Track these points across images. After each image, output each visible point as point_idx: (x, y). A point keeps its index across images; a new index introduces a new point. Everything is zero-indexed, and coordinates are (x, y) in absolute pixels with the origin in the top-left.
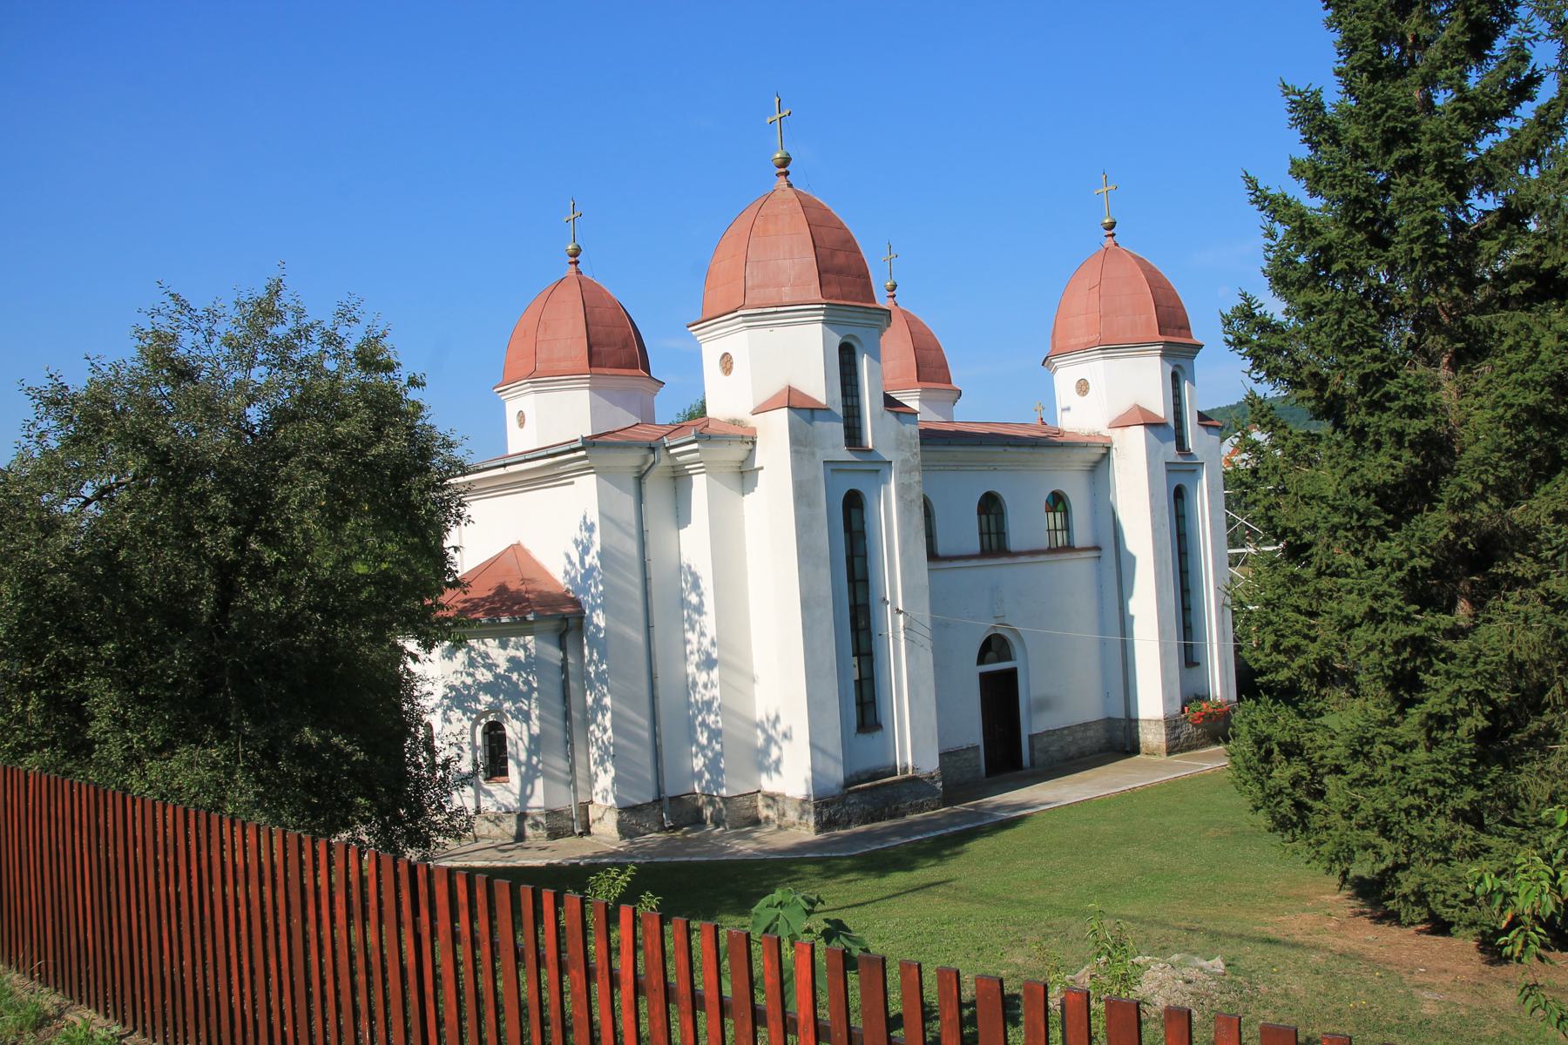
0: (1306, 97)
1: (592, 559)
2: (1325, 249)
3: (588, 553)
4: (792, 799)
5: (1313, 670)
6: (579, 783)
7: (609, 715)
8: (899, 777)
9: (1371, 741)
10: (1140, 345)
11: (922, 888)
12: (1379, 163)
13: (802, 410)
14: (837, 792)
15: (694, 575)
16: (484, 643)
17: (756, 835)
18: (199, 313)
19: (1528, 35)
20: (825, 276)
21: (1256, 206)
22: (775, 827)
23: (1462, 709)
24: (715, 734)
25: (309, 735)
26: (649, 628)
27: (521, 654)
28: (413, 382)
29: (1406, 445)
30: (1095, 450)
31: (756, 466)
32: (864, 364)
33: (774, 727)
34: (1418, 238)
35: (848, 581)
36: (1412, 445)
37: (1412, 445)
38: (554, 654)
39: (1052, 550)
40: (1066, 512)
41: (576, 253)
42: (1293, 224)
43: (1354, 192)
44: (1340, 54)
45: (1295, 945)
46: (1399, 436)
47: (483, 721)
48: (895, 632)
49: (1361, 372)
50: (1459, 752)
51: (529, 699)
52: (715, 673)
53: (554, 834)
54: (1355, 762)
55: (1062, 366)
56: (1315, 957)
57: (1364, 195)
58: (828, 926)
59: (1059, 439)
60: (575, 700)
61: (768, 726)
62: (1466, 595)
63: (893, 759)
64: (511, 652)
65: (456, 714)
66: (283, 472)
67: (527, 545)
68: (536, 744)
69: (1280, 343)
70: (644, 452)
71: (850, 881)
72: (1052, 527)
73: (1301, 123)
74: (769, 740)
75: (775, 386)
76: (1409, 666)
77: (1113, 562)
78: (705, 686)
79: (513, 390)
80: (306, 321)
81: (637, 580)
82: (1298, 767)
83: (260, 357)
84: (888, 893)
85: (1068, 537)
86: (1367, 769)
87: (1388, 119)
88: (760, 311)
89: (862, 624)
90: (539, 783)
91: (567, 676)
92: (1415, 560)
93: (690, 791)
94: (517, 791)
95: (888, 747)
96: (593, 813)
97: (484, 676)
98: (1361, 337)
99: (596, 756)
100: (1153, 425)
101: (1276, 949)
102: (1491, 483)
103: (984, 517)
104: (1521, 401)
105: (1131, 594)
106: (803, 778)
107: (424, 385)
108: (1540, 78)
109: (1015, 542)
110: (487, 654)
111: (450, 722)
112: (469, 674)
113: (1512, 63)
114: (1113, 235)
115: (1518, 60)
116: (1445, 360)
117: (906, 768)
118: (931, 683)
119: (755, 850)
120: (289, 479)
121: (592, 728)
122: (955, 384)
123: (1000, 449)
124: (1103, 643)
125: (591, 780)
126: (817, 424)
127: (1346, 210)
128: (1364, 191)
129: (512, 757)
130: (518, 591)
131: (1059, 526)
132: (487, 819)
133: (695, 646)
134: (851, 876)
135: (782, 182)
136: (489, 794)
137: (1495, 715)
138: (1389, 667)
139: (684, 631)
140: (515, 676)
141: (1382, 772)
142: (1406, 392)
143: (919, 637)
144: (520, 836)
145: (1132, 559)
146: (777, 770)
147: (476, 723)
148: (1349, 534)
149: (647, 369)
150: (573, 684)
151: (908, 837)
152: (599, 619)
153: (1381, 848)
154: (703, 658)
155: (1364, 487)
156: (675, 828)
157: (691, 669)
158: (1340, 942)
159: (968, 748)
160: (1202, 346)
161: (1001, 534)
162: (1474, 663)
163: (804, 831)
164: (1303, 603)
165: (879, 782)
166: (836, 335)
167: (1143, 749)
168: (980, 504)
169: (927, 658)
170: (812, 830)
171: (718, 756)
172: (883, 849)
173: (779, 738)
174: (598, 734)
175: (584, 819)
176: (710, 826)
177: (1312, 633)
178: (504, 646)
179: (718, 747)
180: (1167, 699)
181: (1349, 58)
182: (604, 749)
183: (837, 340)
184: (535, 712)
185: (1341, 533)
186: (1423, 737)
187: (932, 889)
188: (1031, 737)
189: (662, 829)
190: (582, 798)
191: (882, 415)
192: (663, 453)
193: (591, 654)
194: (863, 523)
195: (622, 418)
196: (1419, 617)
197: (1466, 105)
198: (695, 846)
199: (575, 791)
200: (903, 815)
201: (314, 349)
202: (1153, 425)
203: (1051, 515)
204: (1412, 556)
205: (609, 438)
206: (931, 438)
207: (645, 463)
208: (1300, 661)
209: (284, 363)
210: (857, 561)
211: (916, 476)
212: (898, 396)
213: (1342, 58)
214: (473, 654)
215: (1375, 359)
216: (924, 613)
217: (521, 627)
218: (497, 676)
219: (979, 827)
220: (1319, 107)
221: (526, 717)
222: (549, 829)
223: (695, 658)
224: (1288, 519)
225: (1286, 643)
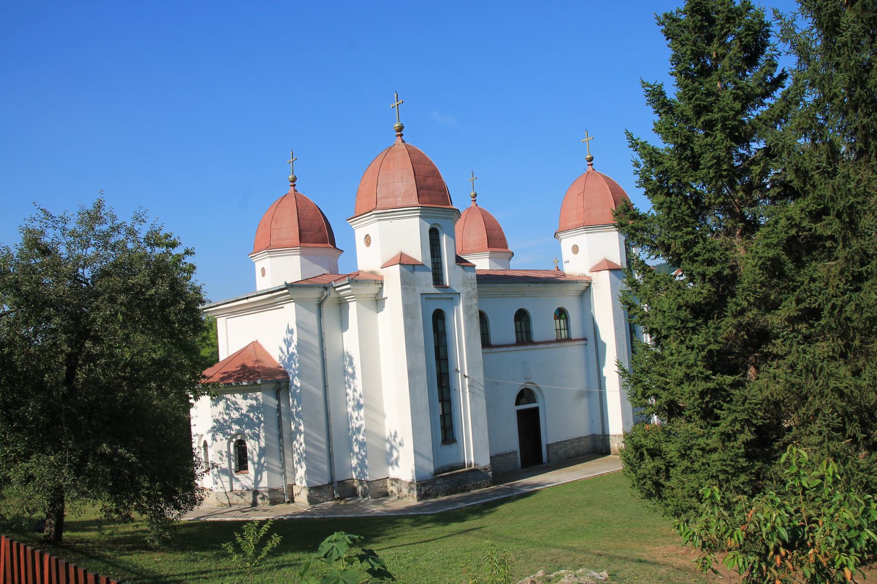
1: (292, 349)
3: (290, 346)
4: (405, 482)
5: (664, 408)
6: (287, 474)
7: (303, 436)
8: (466, 469)
9: (690, 448)
11: (466, 531)
13: (407, 265)
14: (430, 478)
15: (350, 357)
16: (234, 396)
17: (385, 502)
19: (775, 53)
20: (421, 191)
21: (632, 149)
23: (737, 430)
24: (362, 445)
25: (105, 448)
26: (325, 387)
27: (254, 402)
28: (187, 252)
30: (581, 285)
31: (384, 297)
32: (444, 239)
34: (712, 166)
35: (436, 360)
36: (711, 280)
38: (273, 402)
39: (558, 341)
40: (567, 319)
41: (294, 180)
43: (679, 141)
44: (672, 65)
46: (703, 276)
47: (234, 440)
49: (682, 240)
50: (735, 455)
51: (259, 427)
52: (362, 412)
53: (273, 502)
55: (565, 238)
56: (663, 570)
59: (563, 279)
61: (391, 439)
62: (753, 364)
65: (220, 436)
67: (261, 342)
68: (262, 452)
70: (321, 290)
72: (558, 327)
74: (392, 447)
75: (394, 253)
76: (710, 405)
77: (594, 348)
78: (357, 419)
80: (118, 222)
81: (318, 360)
82: (659, 463)
83: (93, 242)
84: (446, 534)
85: (568, 333)
86: (689, 464)
87: (696, 100)
88: (384, 211)
89: (444, 384)
90: (265, 474)
91: (280, 415)
94: (253, 478)
95: (460, 452)
96: (296, 490)
97: (235, 415)
98: (682, 222)
100: (614, 270)
101: (643, 566)
103: (518, 323)
104: (766, 255)
105: (604, 365)
107: (194, 253)
108: (787, 76)
109: (536, 336)
111: (216, 441)
112: (227, 414)
113: (767, 68)
114: (592, 165)
115: (770, 66)
116: (738, 233)
117: (471, 464)
119: (382, 511)
120: (98, 308)
121: (295, 442)
122: (510, 248)
123: (526, 285)
125: (294, 471)
126: (417, 273)
127: (677, 149)
129: (250, 460)
130: (254, 367)
131: (562, 327)
132: (236, 494)
133: (352, 397)
134: (428, 525)
135: (399, 140)
136: (237, 480)
137: (759, 430)
138: (698, 406)
139: (346, 389)
140: (251, 415)
141: (696, 466)
143: (477, 391)
144: (254, 504)
145: (604, 345)
146: (397, 464)
147: (230, 441)
148: (678, 332)
149: (333, 243)
150: (284, 418)
151: (469, 503)
152: (297, 382)
154: (356, 403)
155: (685, 305)
156: (341, 499)
157: (350, 410)
158: (680, 561)
161: (528, 332)
162: (743, 403)
165: (454, 472)
167: (612, 452)
169: (482, 402)
170: (416, 499)
174: (297, 446)
175: (291, 493)
177: (667, 387)
178: (245, 398)
180: (625, 423)
182: (300, 455)
183: (428, 226)
184: (262, 434)
186: (721, 445)
187: (471, 532)
188: (548, 446)
189: (334, 499)
190: (289, 482)
191: (455, 267)
192: (332, 290)
193: (293, 402)
194: (445, 327)
195: (318, 270)
196: (714, 377)
197: (738, 91)
198: (350, 509)
199: (285, 478)
200: (469, 490)
201: (122, 237)
203: (558, 321)
204: (709, 343)
206: (484, 279)
207: (322, 296)
209: (105, 245)
210: (441, 349)
211: (475, 301)
215: (688, 233)
216: (480, 377)
217: (254, 387)
218: (242, 414)
219: (510, 497)
220: (662, 93)
221: (257, 437)
222: (270, 499)
223: (351, 403)
224: (653, 323)
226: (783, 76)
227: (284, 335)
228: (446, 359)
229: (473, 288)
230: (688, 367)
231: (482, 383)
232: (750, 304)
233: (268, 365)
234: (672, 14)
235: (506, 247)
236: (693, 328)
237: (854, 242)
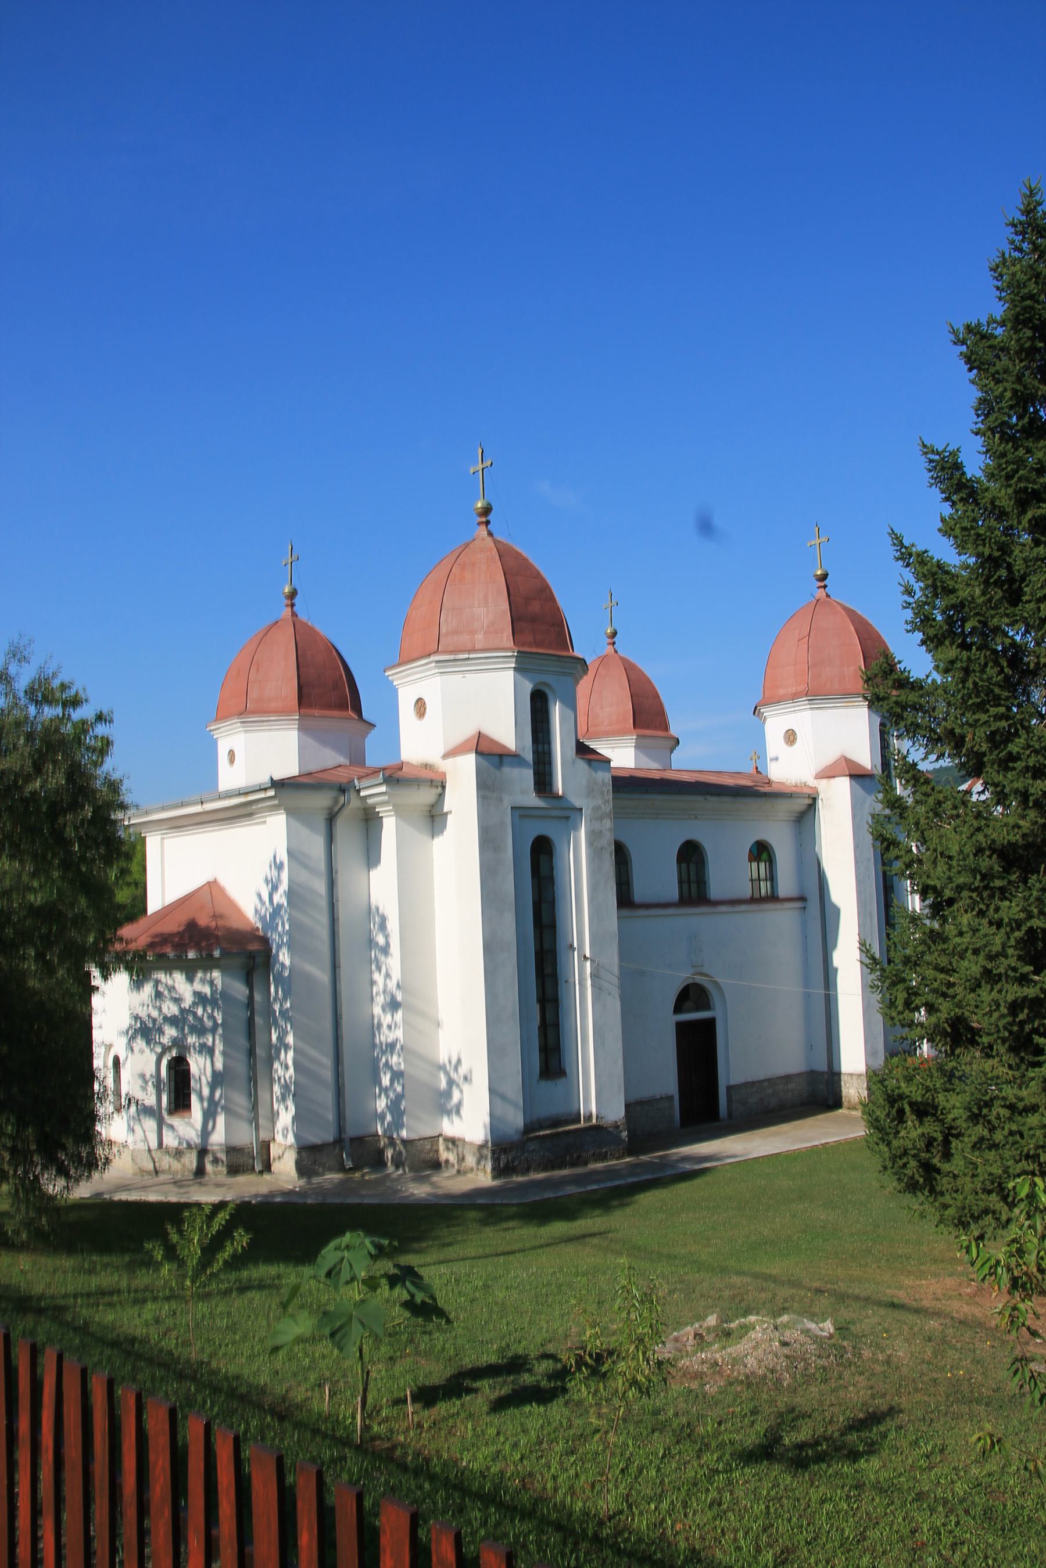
0: (944, 457)
1: (280, 898)
2: (959, 607)
4: (471, 1144)
6: (261, 1121)
7: (291, 1054)
9: (989, 1104)
10: (845, 695)
12: (1015, 523)
14: (516, 1138)
21: (901, 563)
22: (454, 1171)
26: (335, 967)
27: (207, 990)
29: (1031, 804)
32: (557, 712)
33: (456, 1069)
38: (240, 990)
39: (755, 900)
40: (771, 861)
41: (293, 594)
42: (926, 582)
44: (978, 416)
45: (917, 1311)
52: (399, 1016)
53: (234, 1170)
54: (975, 1125)
56: (933, 1324)
57: (997, 554)
58: (396, 1271)
59: (766, 789)
60: (260, 1038)
63: (577, 1107)
64: (198, 986)
67: (223, 882)
68: (218, 1078)
69: (916, 700)
70: (333, 794)
71: (507, 1229)
72: (755, 876)
73: (941, 482)
74: (451, 1082)
75: (466, 731)
76: (1028, 1028)
81: (324, 919)
82: (931, 1128)
87: (1020, 479)
89: (548, 970)
90: (221, 1120)
92: (1033, 921)
93: (373, 1131)
94: (199, 1125)
95: (572, 1093)
96: (274, 1151)
97: (170, 1009)
98: (987, 695)
99: (279, 1093)
100: (858, 776)
101: (897, 1314)
103: (684, 866)
105: (835, 946)
106: (481, 1125)
109: (716, 889)
110: (174, 988)
118: (618, 1031)
122: (674, 731)
123: (701, 798)
124: (807, 996)
125: (274, 1116)
127: (982, 565)
128: (998, 550)
129: (195, 1091)
130: (208, 928)
131: (763, 875)
134: (511, 1224)
135: (483, 531)
138: (1005, 1028)
139: (371, 972)
140: (200, 1011)
142: (1028, 752)
144: (200, 1171)
145: (837, 911)
146: (458, 1112)
148: (974, 895)
149: (357, 708)
150: (258, 1020)
152: (284, 957)
153: (1000, 1213)
154: (388, 1000)
157: (377, 1010)
158: (966, 1309)
159: (661, 1098)
160: (375, 726)
161: (702, 882)
163: (481, 1175)
164: (943, 961)
165: (561, 1129)
171: (399, 1098)
172: (556, 1198)
173: (461, 1081)
176: (390, 1168)
177: (951, 992)
178: (190, 979)
179: (399, 1089)
180: (870, 1052)
181: (986, 419)
182: (286, 1087)
183: (528, 687)
184: (219, 1047)
185: (965, 894)
188: (729, 1088)
189: (342, 1168)
190: (264, 1135)
191: (574, 762)
193: (277, 992)
194: (552, 869)
195: (330, 758)
196: (1036, 978)
200: (586, 1164)
202: (858, 776)
203: (754, 865)
204: (1030, 916)
210: (544, 906)
211: (608, 824)
212: (593, 745)
213: (980, 419)
215: (999, 717)
216: (612, 959)
217: (207, 963)
218: (182, 1011)
220: (958, 466)
221: (211, 1051)
223: (380, 1000)
224: (928, 876)
229: (605, 800)
230: (991, 958)
233: (235, 924)
234: (979, 325)
235: (666, 728)
236: (1002, 890)
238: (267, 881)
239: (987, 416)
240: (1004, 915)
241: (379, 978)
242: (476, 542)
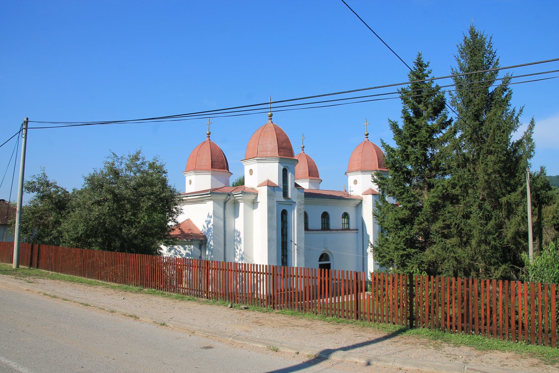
10: (305, 178)
13: (271, 187)
18: (119, 157)
20: (280, 150)
31: (258, 201)
32: (290, 175)
34: (414, 160)
37: (408, 209)
39: (343, 230)
40: (348, 218)
41: (209, 134)
48: (294, 250)
64: (187, 251)
66: (142, 200)
67: (191, 219)
70: (227, 196)
72: (343, 223)
75: (264, 179)
79: (189, 173)
80: (145, 161)
85: (348, 226)
87: (410, 131)
100: (374, 194)
102: (425, 219)
103: (323, 219)
109: (332, 226)
110: (180, 251)
114: (367, 137)
122: (320, 178)
123: (329, 200)
124: (357, 258)
131: (346, 223)
133: (238, 253)
135: (270, 121)
148: (394, 230)
149: (228, 169)
154: (241, 256)
161: (328, 224)
166: (282, 166)
168: (322, 215)
178: (185, 249)
183: (282, 168)
193: (209, 253)
194: (287, 219)
197: (428, 129)
203: (343, 219)
204: (407, 235)
205: (216, 191)
206: (309, 195)
207: (227, 199)
208: (385, 260)
210: (284, 230)
214: (176, 251)
215: (401, 189)
216: (302, 245)
223: (238, 257)
225: (381, 255)
226: (451, 121)
227: (206, 218)
228: (286, 235)
230: (397, 244)
231: (303, 248)
232: (424, 220)
233: (196, 232)
234: (405, 89)
235: (318, 177)
236: (401, 228)
237: (467, 198)
238: (206, 221)
239: (404, 114)
240: (401, 235)
241: (238, 251)
242: (268, 125)
